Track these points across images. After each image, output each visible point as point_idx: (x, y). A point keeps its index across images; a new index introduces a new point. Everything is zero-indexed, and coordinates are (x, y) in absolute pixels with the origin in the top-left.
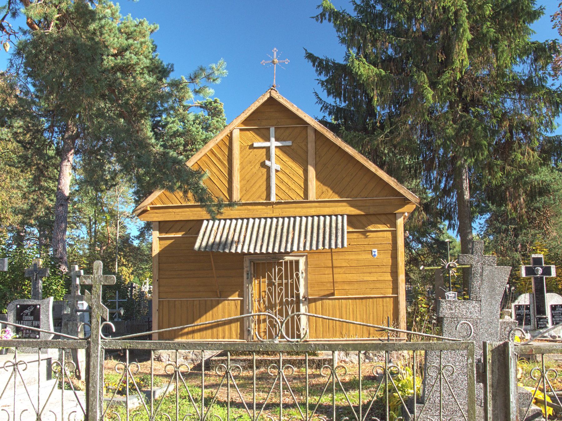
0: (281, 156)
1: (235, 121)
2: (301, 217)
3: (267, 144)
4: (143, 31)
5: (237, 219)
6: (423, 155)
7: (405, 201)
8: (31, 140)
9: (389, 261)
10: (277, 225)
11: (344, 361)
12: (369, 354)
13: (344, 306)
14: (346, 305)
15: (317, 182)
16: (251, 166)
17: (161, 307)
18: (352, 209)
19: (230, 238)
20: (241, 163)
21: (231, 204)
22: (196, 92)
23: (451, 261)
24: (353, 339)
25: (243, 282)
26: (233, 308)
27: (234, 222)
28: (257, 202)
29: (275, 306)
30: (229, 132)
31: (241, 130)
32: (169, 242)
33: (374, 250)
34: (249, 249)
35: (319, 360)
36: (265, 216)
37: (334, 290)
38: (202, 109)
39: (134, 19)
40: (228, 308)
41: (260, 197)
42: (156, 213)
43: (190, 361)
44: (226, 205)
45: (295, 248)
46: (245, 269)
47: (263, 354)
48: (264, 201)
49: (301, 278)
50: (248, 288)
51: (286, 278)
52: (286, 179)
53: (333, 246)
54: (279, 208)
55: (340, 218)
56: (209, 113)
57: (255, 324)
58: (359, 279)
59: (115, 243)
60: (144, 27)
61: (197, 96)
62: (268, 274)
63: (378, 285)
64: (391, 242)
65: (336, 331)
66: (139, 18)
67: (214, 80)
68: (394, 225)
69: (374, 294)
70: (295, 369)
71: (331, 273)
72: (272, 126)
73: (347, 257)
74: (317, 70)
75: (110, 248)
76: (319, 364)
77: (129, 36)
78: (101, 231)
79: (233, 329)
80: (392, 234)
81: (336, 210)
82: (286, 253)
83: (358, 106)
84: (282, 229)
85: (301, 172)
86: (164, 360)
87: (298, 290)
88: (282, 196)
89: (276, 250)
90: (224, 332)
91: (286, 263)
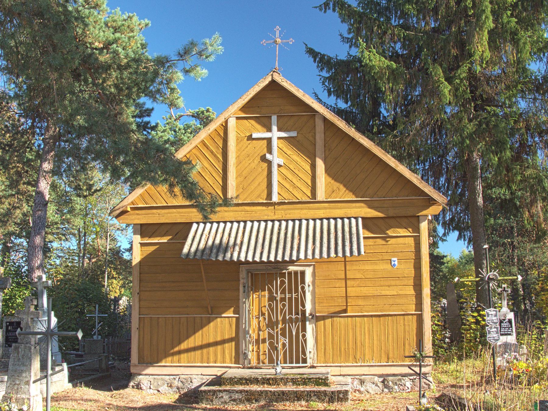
0: (285, 149)
1: (230, 107)
2: (307, 220)
3: (268, 135)
4: (132, 26)
5: (232, 222)
6: (430, 161)
7: (431, 202)
8: (11, 142)
9: (412, 272)
10: (280, 229)
11: (359, 391)
12: (388, 382)
13: (358, 325)
14: (361, 324)
15: (328, 177)
16: (249, 160)
17: (142, 325)
18: (370, 210)
19: (225, 240)
20: (238, 157)
21: (226, 202)
22: (186, 72)
23: (491, 271)
24: (369, 364)
25: (239, 295)
26: (227, 326)
27: (229, 225)
28: (256, 202)
29: (277, 322)
30: (223, 120)
31: (238, 118)
32: (152, 248)
33: (393, 259)
34: (246, 257)
35: (333, 392)
36: (266, 218)
37: (347, 306)
38: (194, 118)
39: (123, 13)
40: (222, 326)
41: (259, 196)
42: (138, 214)
43: (175, 389)
44: (220, 205)
45: (302, 256)
46: (242, 281)
47: (263, 383)
48: (265, 201)
49: (307, 291)
50: (245, 303)
51: (290, 292)
52: (290, 176)
53: (348, 254)
54: (282, 209)
55: (353, 221)
56: (201, 122)
57: (253, 346)
58: (376, 293)
59: (105, 256)
60: (133, 21)
61: (187, 76)
62: (268, 287)
63: (398, 301)
64: (413, 250)
65: (349, 354)
66: (128, 13)
67: (207, 57)
68: (417, 229)
69: (394, 311)
70: (303, 403)
71: (344, 286)
72: (275, 114)
73: (362, 267)
74: (318, 66)
75: (100, 261)
76: (332, 397)
77: (116, 30)
78: (91, 243)
79: (227, 352)
80: (415, 240)
81: (349, 212)
82: (292, 262)
83: (362, 106)
84: (286, 234)
85: (308, 168)
86: (144, 388)
87: (303, 306)
88: (285, 195)
89: (279, 258)
90: (216, 355)
91: (290, 273)
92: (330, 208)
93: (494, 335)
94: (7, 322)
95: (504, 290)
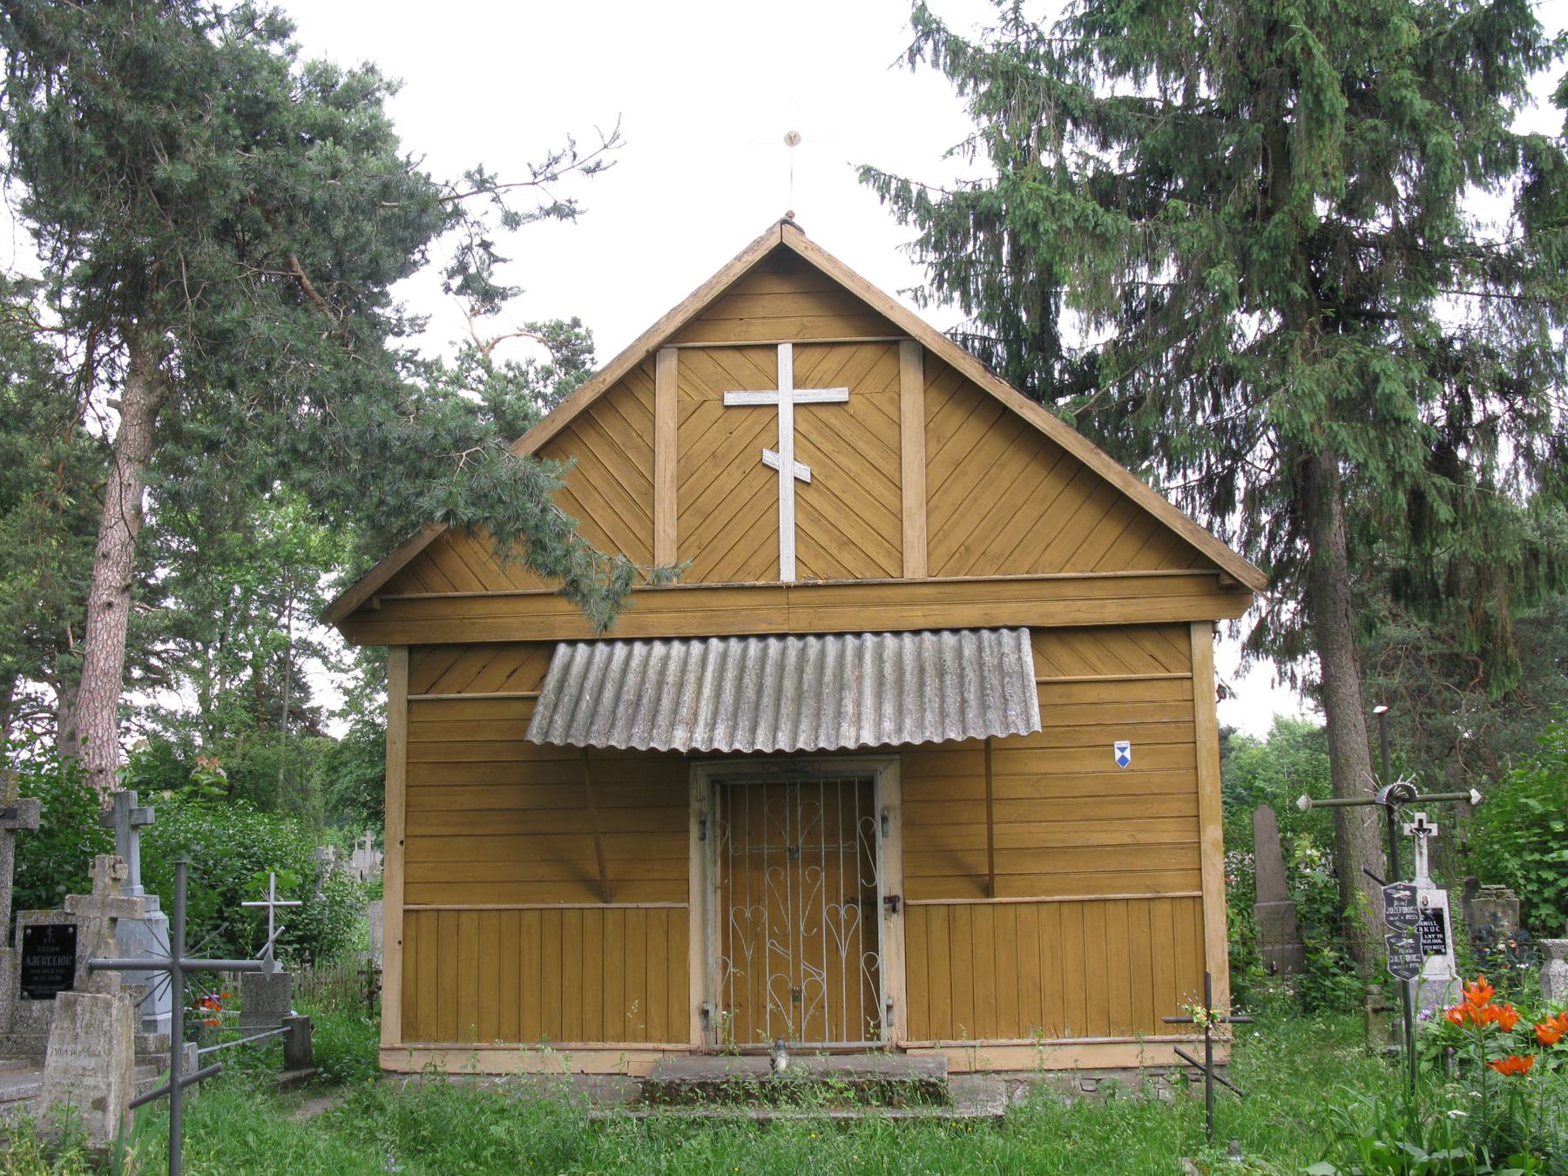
46: (695, 806)
52: (830, 512)
88: (817, 565)
92: (936, 601)
93: (1408, 958)
94: (26, 928)
95: (1421, 828)
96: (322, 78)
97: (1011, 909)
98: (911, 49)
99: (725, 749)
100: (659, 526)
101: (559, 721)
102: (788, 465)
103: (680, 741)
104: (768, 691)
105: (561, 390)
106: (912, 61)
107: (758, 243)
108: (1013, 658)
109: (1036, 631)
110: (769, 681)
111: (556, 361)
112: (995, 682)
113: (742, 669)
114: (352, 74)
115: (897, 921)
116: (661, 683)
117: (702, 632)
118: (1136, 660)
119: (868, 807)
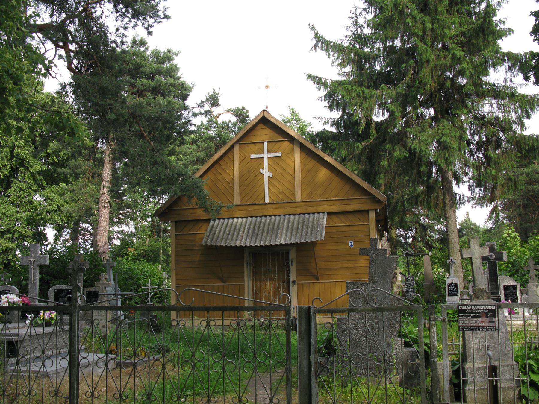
46: (245, 259)
96: (156, 54)
97: (323, 284)
98: (315, 45)
99: (248, 245)
100: (235, 190)
101: (209, 239)
102: (266, 173)
103: (238, 244)
104: (261, 230)
105: (239, 129)
106: (315, 48)
107: (257, 116)
108: (321, 220)
109: (329, 214)
110: (261, 228)
111: (238, 120)
112: (316, 227)
113: (255, 225)
114: (164, 53)
115: (295, 287)
116: (235, 229)
117: (246, 216)
118: (355, 221)
119: (288, 259)
